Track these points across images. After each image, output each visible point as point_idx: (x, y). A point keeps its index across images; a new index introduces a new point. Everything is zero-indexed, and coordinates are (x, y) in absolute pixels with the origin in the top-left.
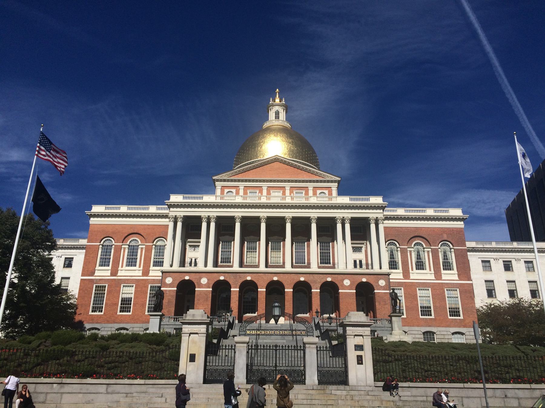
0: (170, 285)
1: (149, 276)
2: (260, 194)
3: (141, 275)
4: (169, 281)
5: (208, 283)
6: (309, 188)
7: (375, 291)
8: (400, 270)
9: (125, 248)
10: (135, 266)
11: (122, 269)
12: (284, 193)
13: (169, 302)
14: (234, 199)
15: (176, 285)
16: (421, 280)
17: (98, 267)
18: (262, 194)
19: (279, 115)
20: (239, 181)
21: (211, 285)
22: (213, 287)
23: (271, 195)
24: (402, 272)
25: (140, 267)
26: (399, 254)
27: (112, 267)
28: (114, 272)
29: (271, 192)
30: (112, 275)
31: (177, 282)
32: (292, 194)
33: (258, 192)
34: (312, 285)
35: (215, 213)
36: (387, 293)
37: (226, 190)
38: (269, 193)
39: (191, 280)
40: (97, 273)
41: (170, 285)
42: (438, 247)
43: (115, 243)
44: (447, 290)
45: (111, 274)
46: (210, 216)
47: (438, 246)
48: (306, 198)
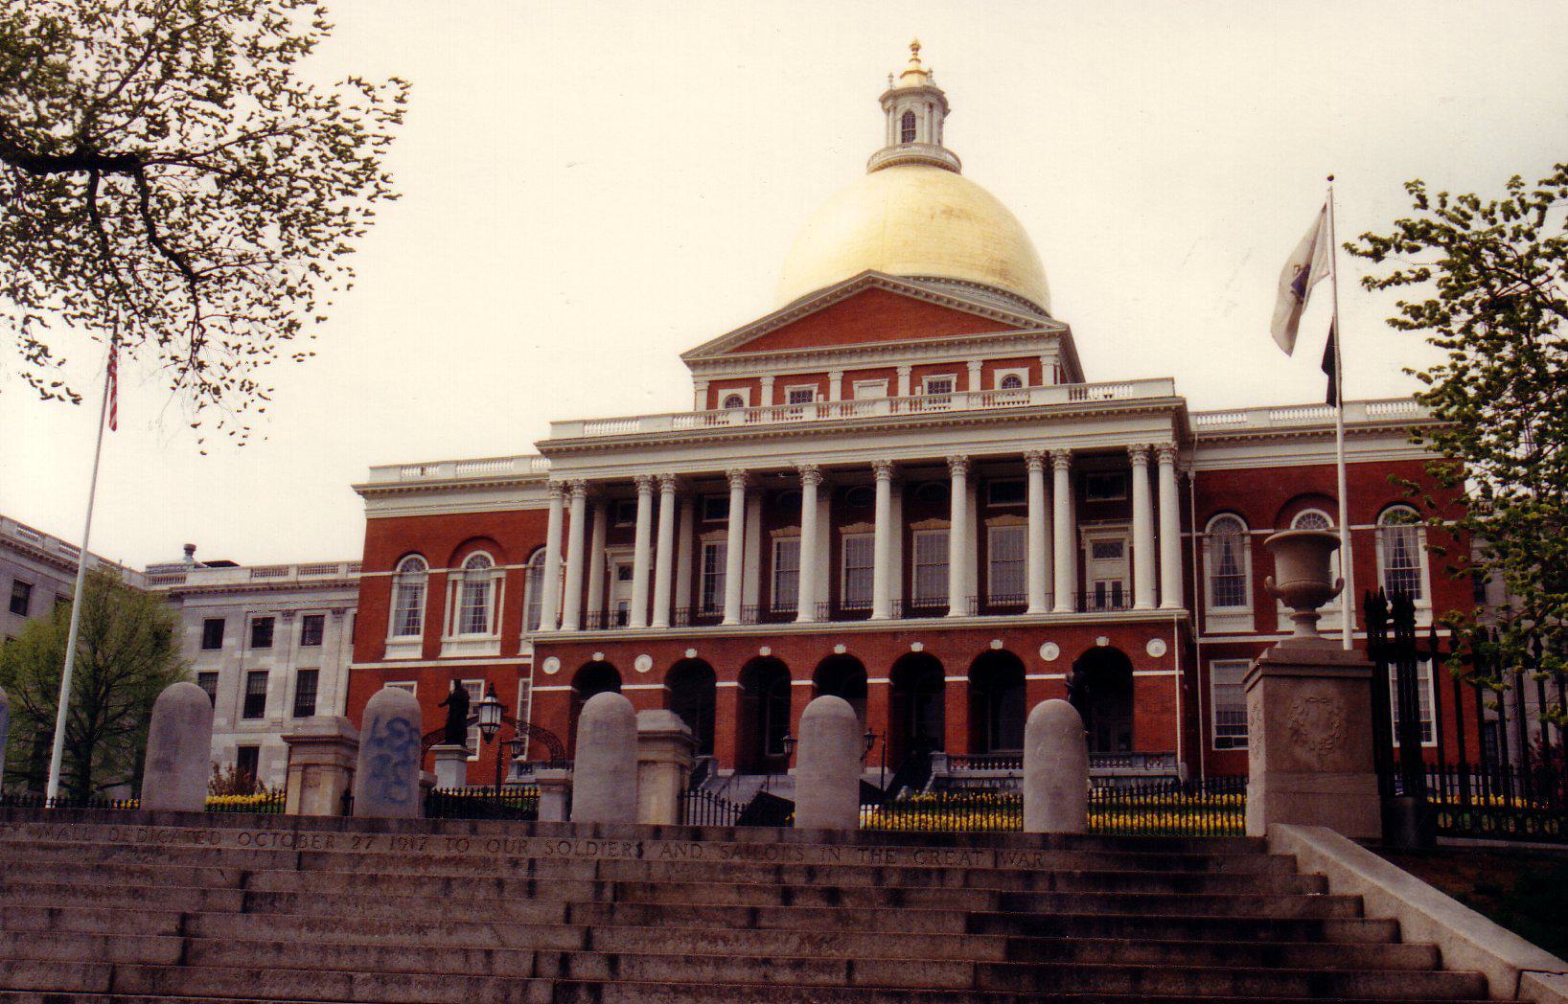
0: (1053, 666)
1: (520, 657)
2: (821, 396)
3: (498, 654)
4: (1050, 652)
5: (654, 669)
6: (832, 377)
7: (870, 681)
8: (1248, 608)
9: (455, 582)
10: (485, 631)
11: (452, 639)
12: (893, 390)
13: (654, 720)
14: (1025, 398)
15: (811, 670)
16: (465, 658)
17: (391, 639)
18: (827, 398)
19: (914, 126)
20: (895, 349)
21: (663, 674)
22: (1076, 667)
23: (856, 399)
24: (1251, 611)
25: (495, 632)
26: (1248, 555)
27: (503, 633)
28: (432, 649)
29: (855, 387)
30: (426, 656)
31: (573, 669)
32: (918, 389)
33: (815, 390)
34: (944, 661)
35: (1064, 441)
36: (880, 684)
37: (1000, 375)
38: (847, 392)
39: (703, 661)
40: (391, 654)
41: (1053, 666)
42: (1373, 527)
43: (431, 568)
44: (1216, 665)
45: (424, 654)
46: (1157, 447)
47: (1376, 523)
48: (984, 399)
